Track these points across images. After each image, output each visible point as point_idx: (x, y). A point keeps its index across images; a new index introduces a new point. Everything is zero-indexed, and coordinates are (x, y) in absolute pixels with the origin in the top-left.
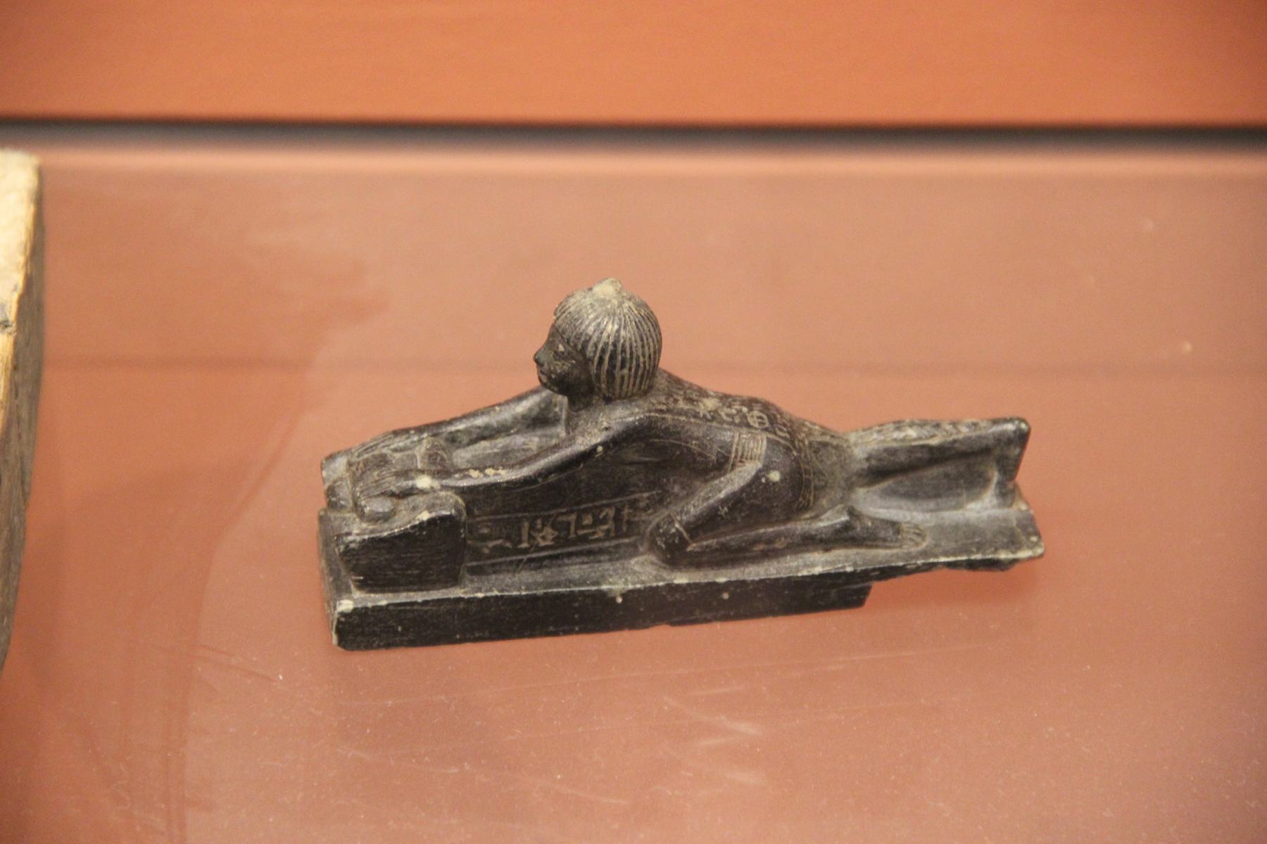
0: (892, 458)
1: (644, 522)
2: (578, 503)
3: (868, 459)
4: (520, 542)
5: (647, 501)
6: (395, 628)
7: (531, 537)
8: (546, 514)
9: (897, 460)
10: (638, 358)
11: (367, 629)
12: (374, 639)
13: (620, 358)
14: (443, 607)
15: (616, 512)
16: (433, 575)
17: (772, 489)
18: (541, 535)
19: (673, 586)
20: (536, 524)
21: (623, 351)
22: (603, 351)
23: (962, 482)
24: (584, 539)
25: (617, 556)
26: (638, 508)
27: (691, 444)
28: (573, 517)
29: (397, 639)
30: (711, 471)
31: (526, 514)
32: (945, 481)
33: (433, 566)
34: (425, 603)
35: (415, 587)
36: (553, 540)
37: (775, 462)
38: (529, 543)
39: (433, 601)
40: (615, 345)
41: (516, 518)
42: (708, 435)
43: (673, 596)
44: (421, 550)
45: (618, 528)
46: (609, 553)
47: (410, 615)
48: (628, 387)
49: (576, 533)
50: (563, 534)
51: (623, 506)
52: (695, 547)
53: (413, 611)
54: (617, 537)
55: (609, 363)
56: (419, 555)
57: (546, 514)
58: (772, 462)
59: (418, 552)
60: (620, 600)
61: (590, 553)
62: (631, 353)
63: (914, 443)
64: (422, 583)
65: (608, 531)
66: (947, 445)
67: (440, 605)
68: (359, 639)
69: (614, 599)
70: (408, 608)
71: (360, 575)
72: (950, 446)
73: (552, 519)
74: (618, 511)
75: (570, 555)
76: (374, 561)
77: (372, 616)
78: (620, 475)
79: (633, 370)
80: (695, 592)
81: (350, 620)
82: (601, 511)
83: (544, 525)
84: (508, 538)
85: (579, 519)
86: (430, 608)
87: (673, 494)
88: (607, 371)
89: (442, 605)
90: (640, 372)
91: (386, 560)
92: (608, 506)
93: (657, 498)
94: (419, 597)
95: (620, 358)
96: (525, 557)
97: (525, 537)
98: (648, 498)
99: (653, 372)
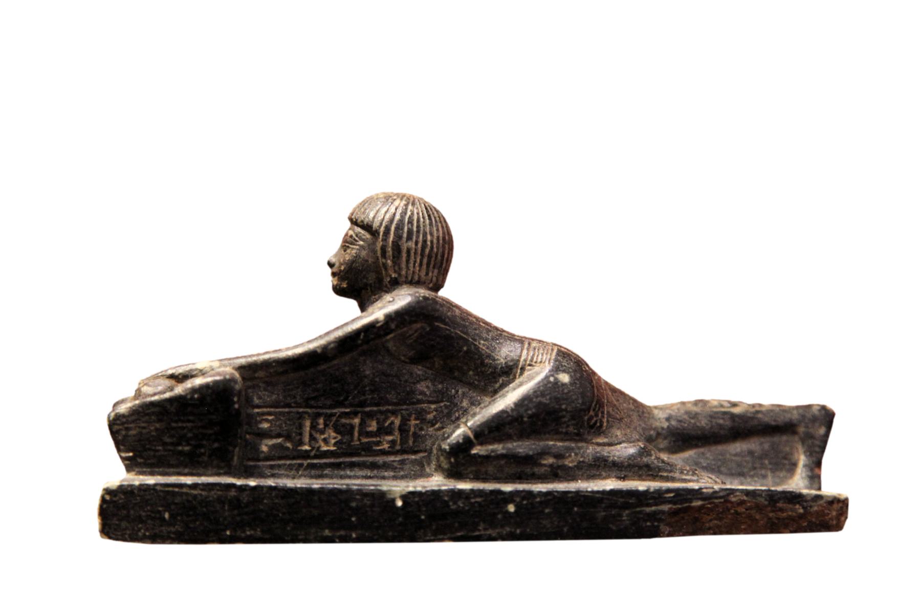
0: (693, 421)
1: (431, 436)
2: (362, 404)
3: (668, 419)
4: (301, 443)
5: (435, 413)
6: (163, 513)
7: (312, 438)
8: (329, 411)
9: (698, 424)
10: (425, 234)
11: (132, 512)
12: (140, 526)
13: (406, 229)
16: (203, 454)
17: (561, 389)
18: (323, 437)
19: (456, 490)
20: (318, 424)
21: (410, 222)
22: (392, 221)
24: (367, 449)
25: (402, 473)
26: (425, 419)
27: (480, 343)
28: (357, 421)
29: (163, 528)
30: (500, 376)
31: (309, 410)
33: (204, 442)
34: (195, 486)
35: (186, 471)
36: (335, 445)
37: (565, 366)
38: (310, 446)
39: (203, 484)
41: (298, 413)
42: (497, 339)
44: (191, 418)
45: (404, 440)
46: (394, 469)
47: (178, 500)
48: (414, 267)
49: (359, 440)
50: (346, 438)
51: (410, 415)
52: (480, 450)
53: (181, 494)
54: (403, 451)
55: (394, 233)
56: (189, 425)
57: (329, 411)
58: (562, 366)
59: (189, 421)
60: (399, 503)
61: (374, 466)
62: (418, 227)
64: (192, 464)
65: (393, 443)
66: (749, 415)
67: (210, 490)
68: (124, 524)
69: (393, 501)
70: (176, 490)
71: (128, 451)
72: (752, 415)
73: (334, 419)
74: (405, 421)
75: (352, 465)
76: (144, 431)
77: (139, 496)
78: (406, 377)
79: (420, 245)
80: (479, 500)
81: (115, 499)
82: (387, 418)
83: (326, 425)
84: (288, 437)
85: (363, 424)
86: (200, 492)
88: (393, 242)
90: (427, 251)
91: (157, 430)
92: (394, 413)
93: (446, 411)
94: (189, 480)
95: (406, 229)
96: (305, 463)
97: (306, 439)
98: (436, 410)
99: (446, 267)
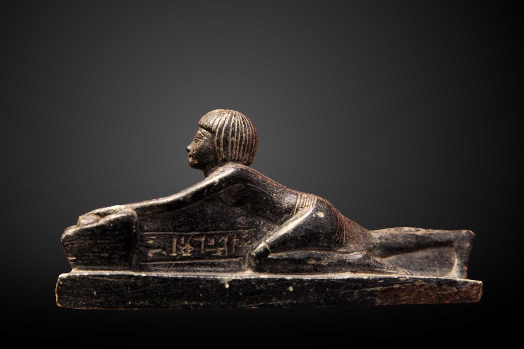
1: (245, 248)
2: (206, 230)
3: (380, 238)
4: (171, 252)
5: (247, 235)
6: (92, 291)
7: (178, 249)
8: (187, 234)
10: (242, 133)
11: (75, 291)
12: (80, 299)
13: (231, 130)
14: (121, 280)
15: (228, 239)
16: (116, 258)
17: (319, 221)
18: (184, 248)
19: (260, 279)
20: (181, 241)
21: (234, 126)
23: (436, 262)
24: (209, 255)
25: (229, 269)
26: (242, 238)
27: (273, 195)
28: (203, 239)
29: (93, 300)
30: (284, 214)
31: (176, 233)
34: (111, 276)
35: (106, 267)
36: (191, 253)
37: (321, 208)
38: (176, 253)
39: (116, 275)
40: (227, 129)
41: (170, 235)
42: (283, 193)
44: (109, 238)
45: (230, 250)
46: (224, 266)
47: (101, 284)
48: (236, 152)
49: (204, 250)
50: (197, 249)
51: (233, 236)
52: (273, 256)
53: (103, 281)
54: (229, 257)
55: (224, 133)
56: (108, 241)
57: (187, 234)
58: (320, 208)
59: (108, 239)
60: (227, 286)
61: (213, 265)
62: (238, 129)
63: (407, 233)
65: (224, 252)
66: (426, 236)
67: (120, 279)
69: (224, 285)
70: (100, 278)
72: (428, 236)
73: (190, 238)
74: (230, 239)
75: (200, 265)
76: (82, 245)
77: (79, 282)
79: (239, 139)
80: (272, 284)
81: (65, 284)
82: (220, 238)
83: (185, 242)
84: (164, 249)
85: (206, 241)
86: (114, 280)
88: (223, 137)
89: (121, 278)
90: (243, 142)
91: (89, 244)
92: (224, 235)
93: (254, 234)
94: (107, 273)
96: (174, 263)
97: (174, 249)
98: (248, 233)
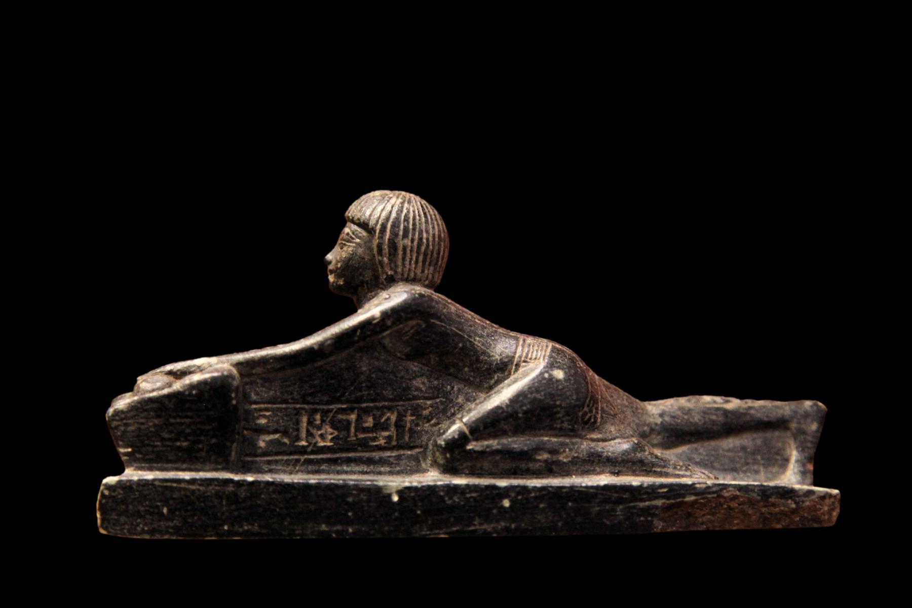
0: (686, 417)
1: (427, 432)
2: (359, 400)
4: (298, 439)
5: (430, 409)
6: (161, 508)
7: (309, 434)
8: (325, 407)
9: (691, 420)
10: (421, 232)
11: (131, 507)
13: (402, 227)
14: (211, 488)
16: (201, 450)
17: (555, 385)
18: (319, 432)
19: (452, 486)
20: (315, 420)
21: (406, 220)
22: (388, 218)
24: (364, 445)
25: (398, 468)
26: (421, 415)
28: (353, 417)
29: (162, 523)
30: (495, 372)
31: (306, 406)
32: (741, 454)
33: (203, 438)
34: (193, 481)
35: (185, 466)
36: (332, 440)
37: (559, 362)
38: (307, 441)
39: (201, 480)
41: (295, 409)
43: (451, 498)
44: (189, 414)
45: (400, 436)
46: (390, 464)
47: (176, 495)
48: (410, 264)
49: (356, 436)
50: (343, 434)
51: (406, 411)
52: (475, 445)
53: (180, 489)
54: (399, 447)
55: (390, 231)
56: (187, 421)
57: (325, 407)
58: (556, 362)
59: (187, 417)
60: (396, 498)
61: (370, 461)
62: (414, 224)
65: (389, 438)
66: (742, 411)
67: (208, 485)
69: (389, 496)
70: (175, 485)
72: (745, 411)
73: (331, 415)
74: (401, 417)
75: (349, 461)
76: (143, 427)
77: (138, 491)
79: (416, 243)
80: (474, 495)
81: (113, 494)
83: (323, 421)
84: (285, 433)
85: (359, 419)
86: (198, 487)
87: (457, 403)
88: (389, 239)
89: (211, 485)
90: (423, 248)
91: (155, 425)
92: (390, 409)
94: (187, 476)
95: (402, 227)
96: (302, 458)
97: (303, 434)
98: (432, 406)
